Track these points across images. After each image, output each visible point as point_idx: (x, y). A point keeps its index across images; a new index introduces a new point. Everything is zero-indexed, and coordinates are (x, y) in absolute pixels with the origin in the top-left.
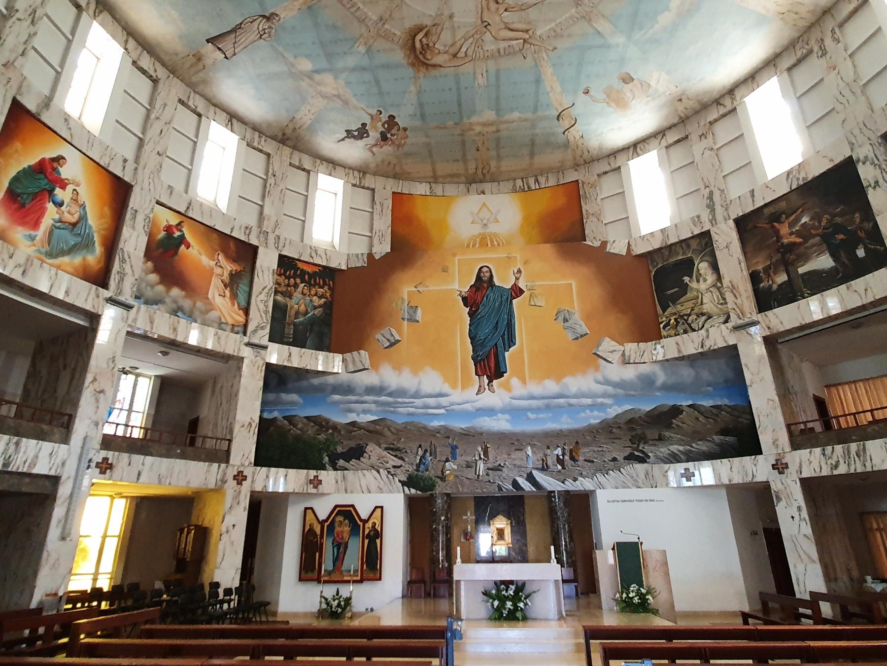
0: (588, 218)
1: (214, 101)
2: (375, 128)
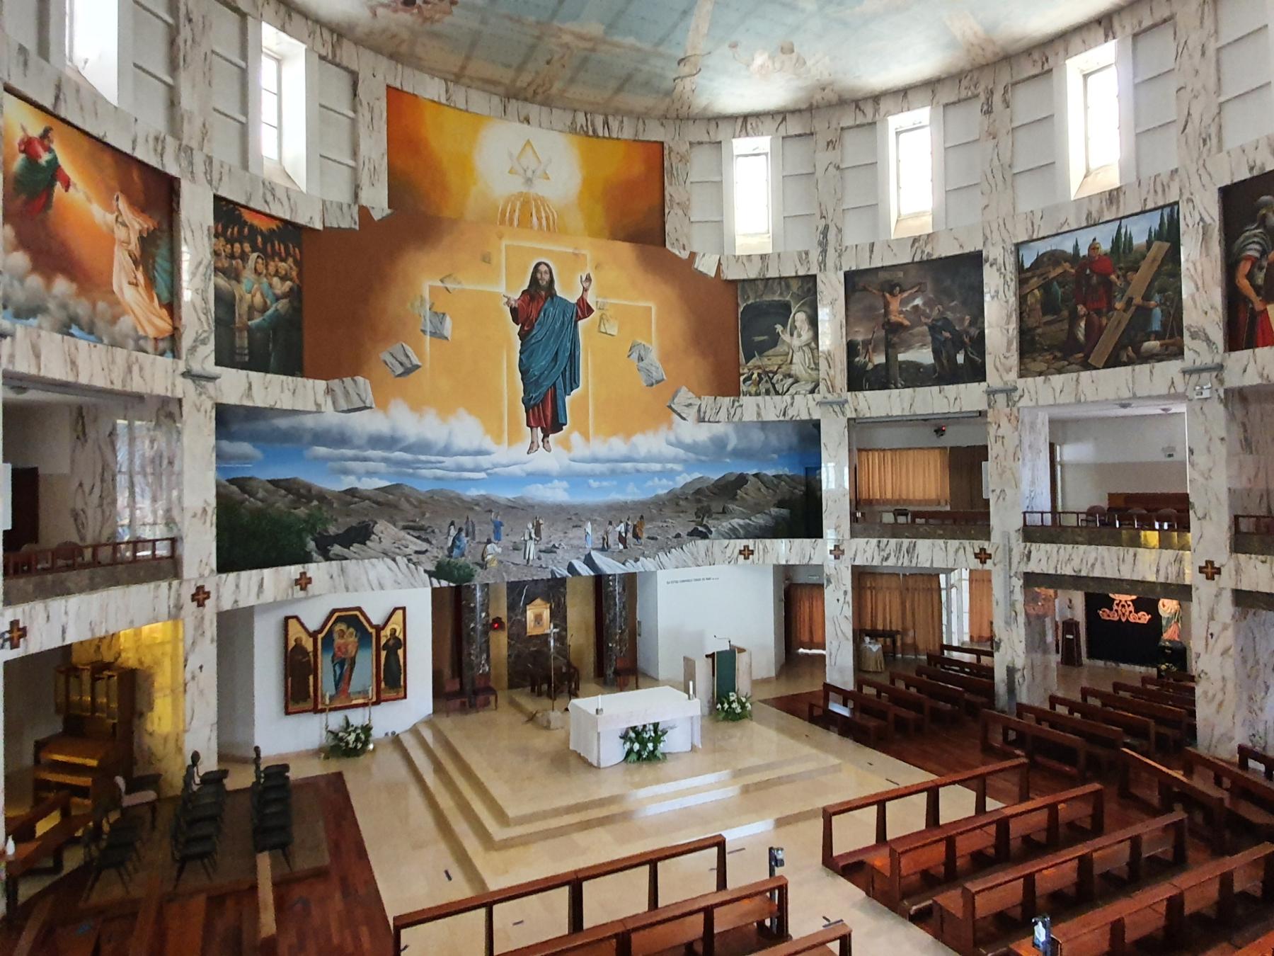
0: (672, 207)
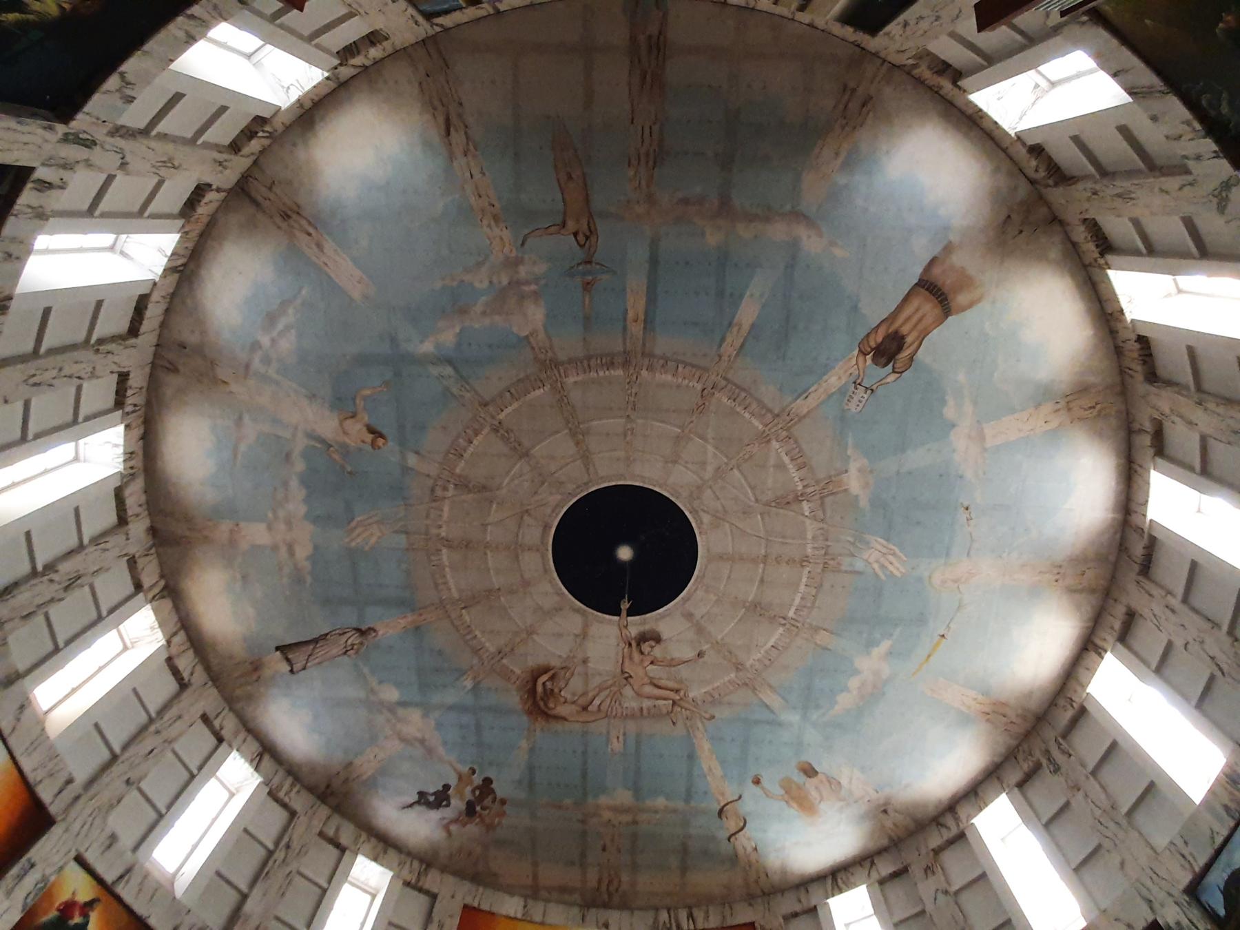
2: (461, 794)
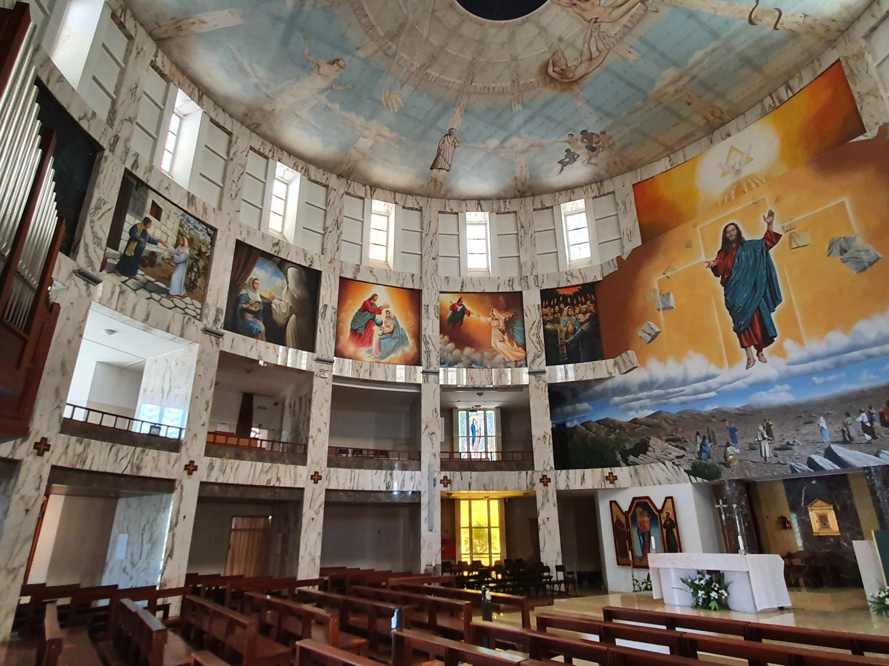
0: (862, 100)
1: (463, 198)
2: (578, 148)
